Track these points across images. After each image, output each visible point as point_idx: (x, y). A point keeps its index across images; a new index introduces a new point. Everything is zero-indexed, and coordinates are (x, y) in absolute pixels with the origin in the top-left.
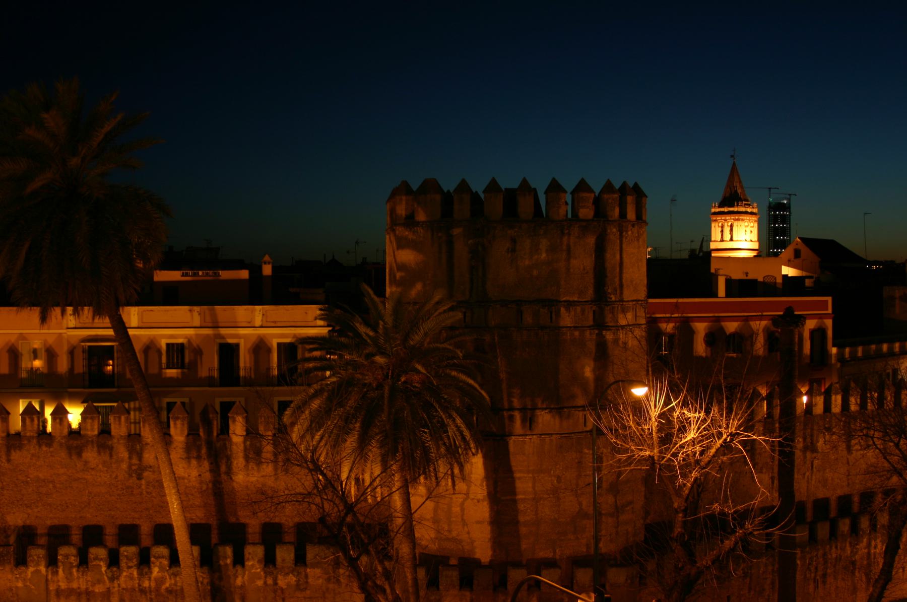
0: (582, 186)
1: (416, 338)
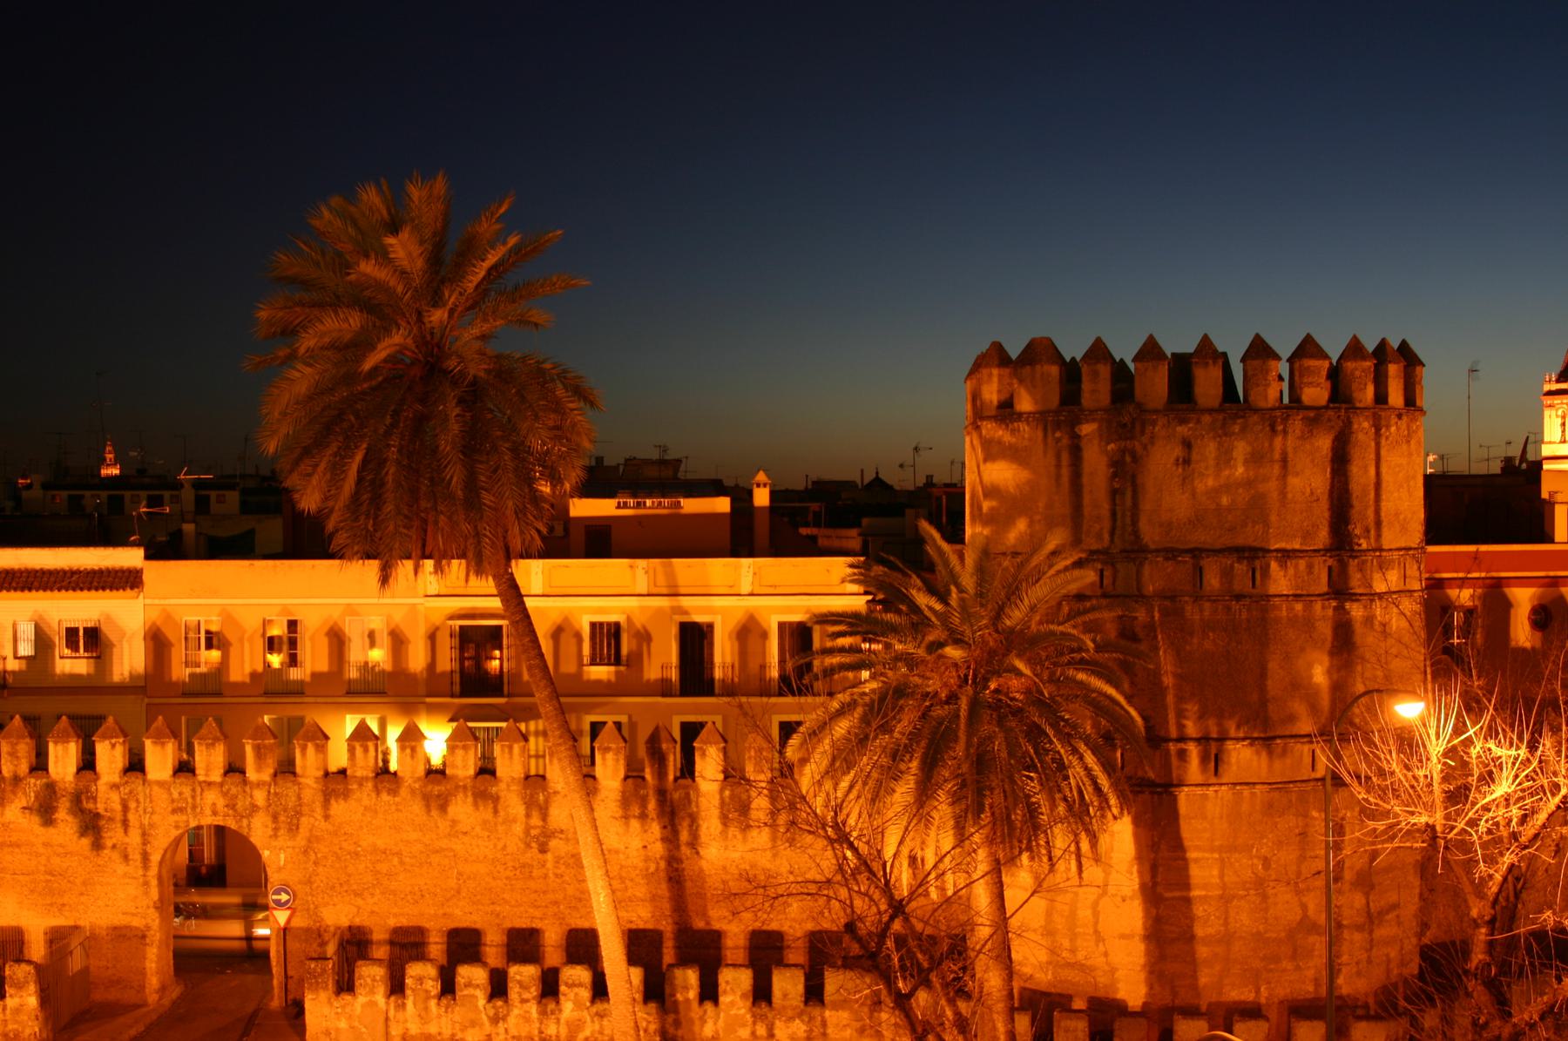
0: (1308, 348)
1: (1015, 617)
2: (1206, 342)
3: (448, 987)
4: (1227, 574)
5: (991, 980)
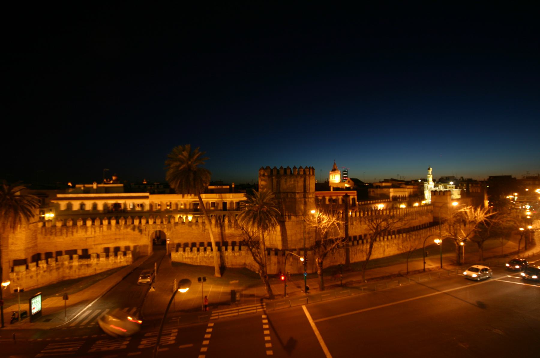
0: (301, 167)
1: (265, 201)
2: (288, 167)
3: (191, 250)
4: (291, 195)
5: (262, 247)
